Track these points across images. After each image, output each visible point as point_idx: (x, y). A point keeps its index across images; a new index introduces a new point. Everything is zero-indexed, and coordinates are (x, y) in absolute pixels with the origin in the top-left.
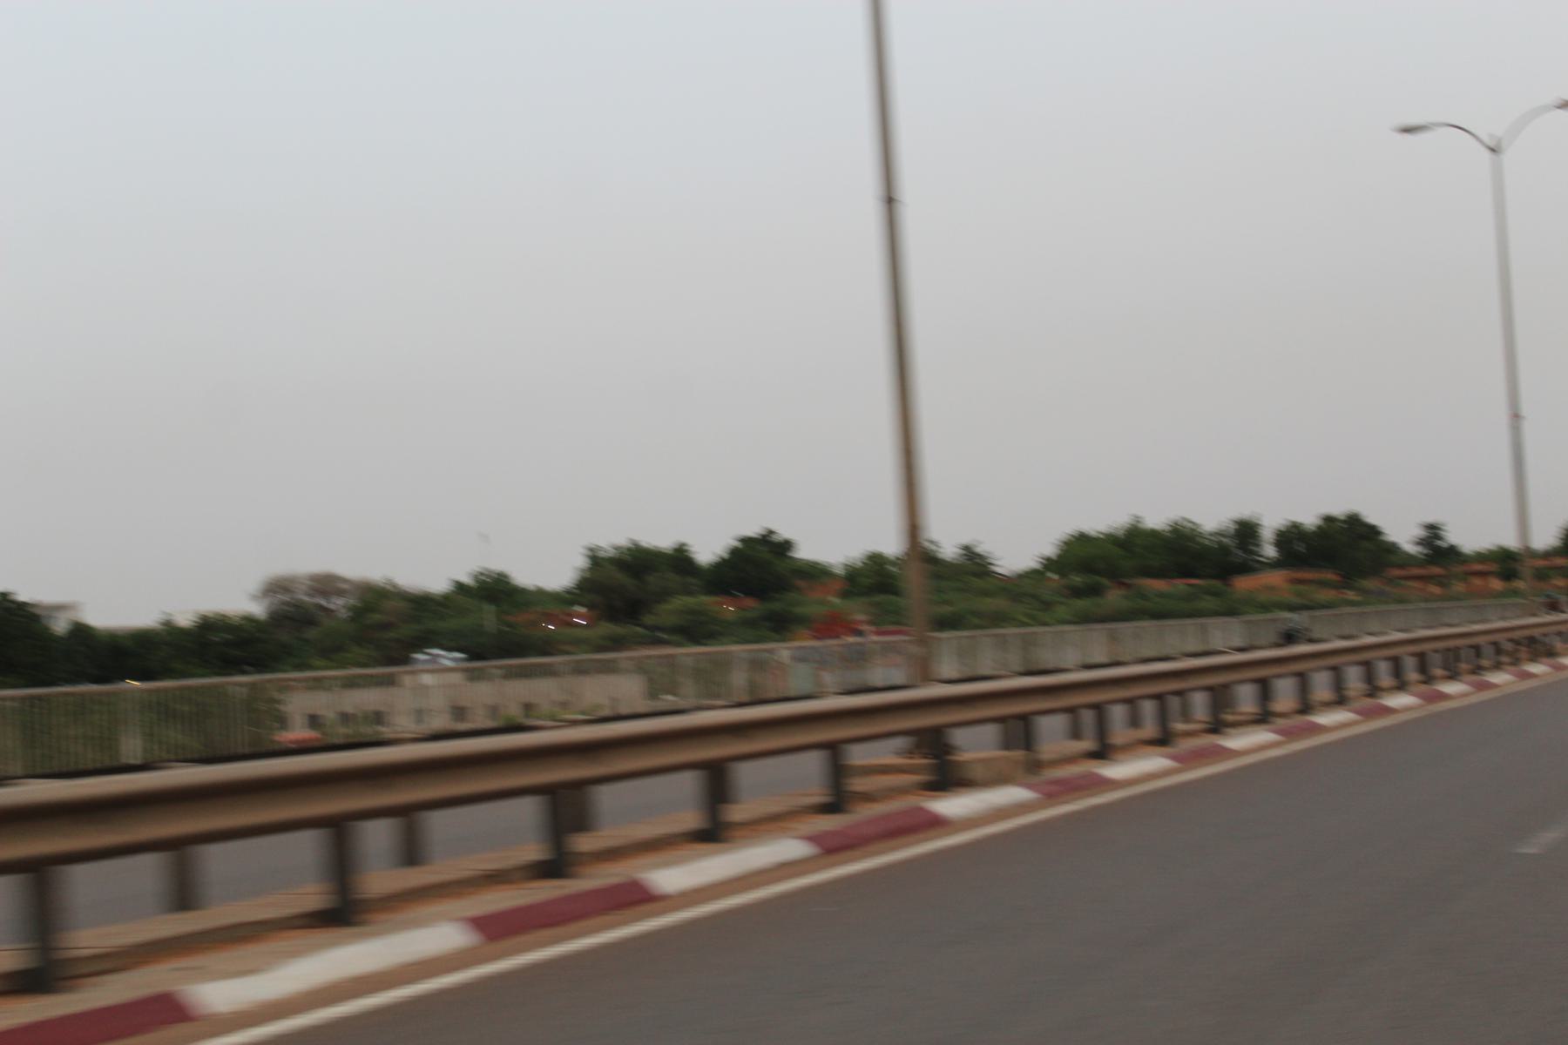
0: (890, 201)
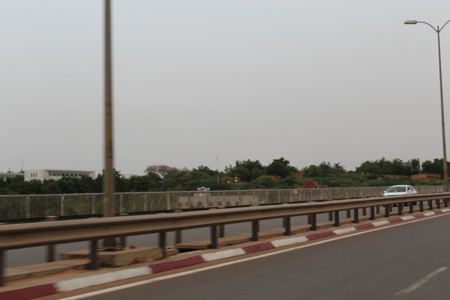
0: (443, 124)
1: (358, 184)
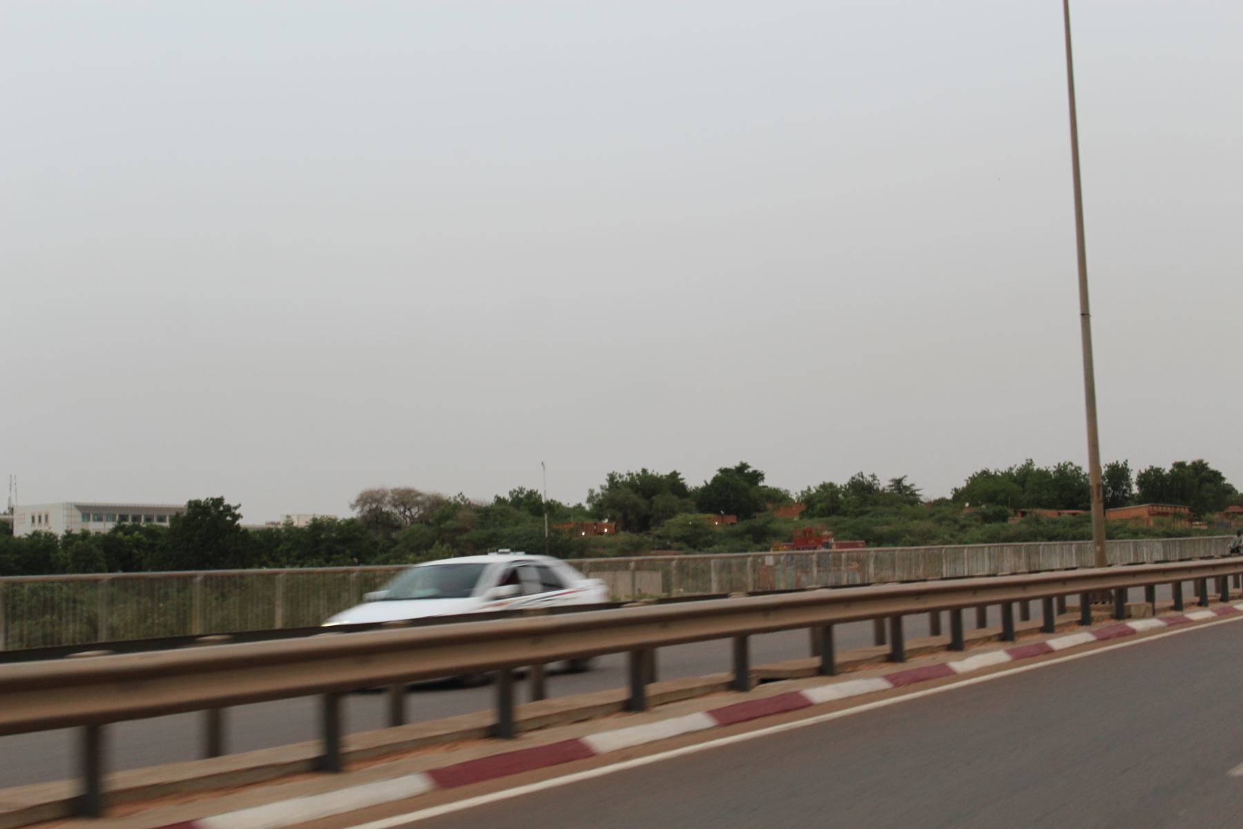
0: (1085, 315)
1: (952, 536)
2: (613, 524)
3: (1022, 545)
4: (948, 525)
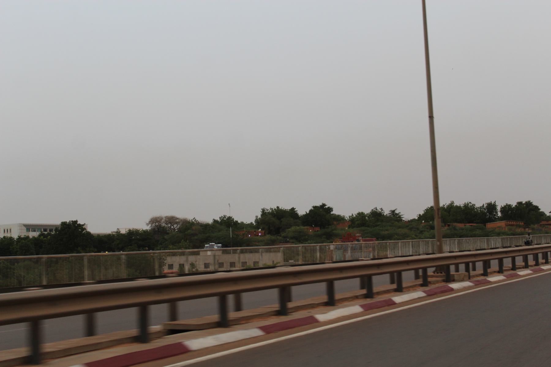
0: (431, 117)
1: (416, 236)
2: (263, 232)
3: (430, 240)
4: (414, 231)
